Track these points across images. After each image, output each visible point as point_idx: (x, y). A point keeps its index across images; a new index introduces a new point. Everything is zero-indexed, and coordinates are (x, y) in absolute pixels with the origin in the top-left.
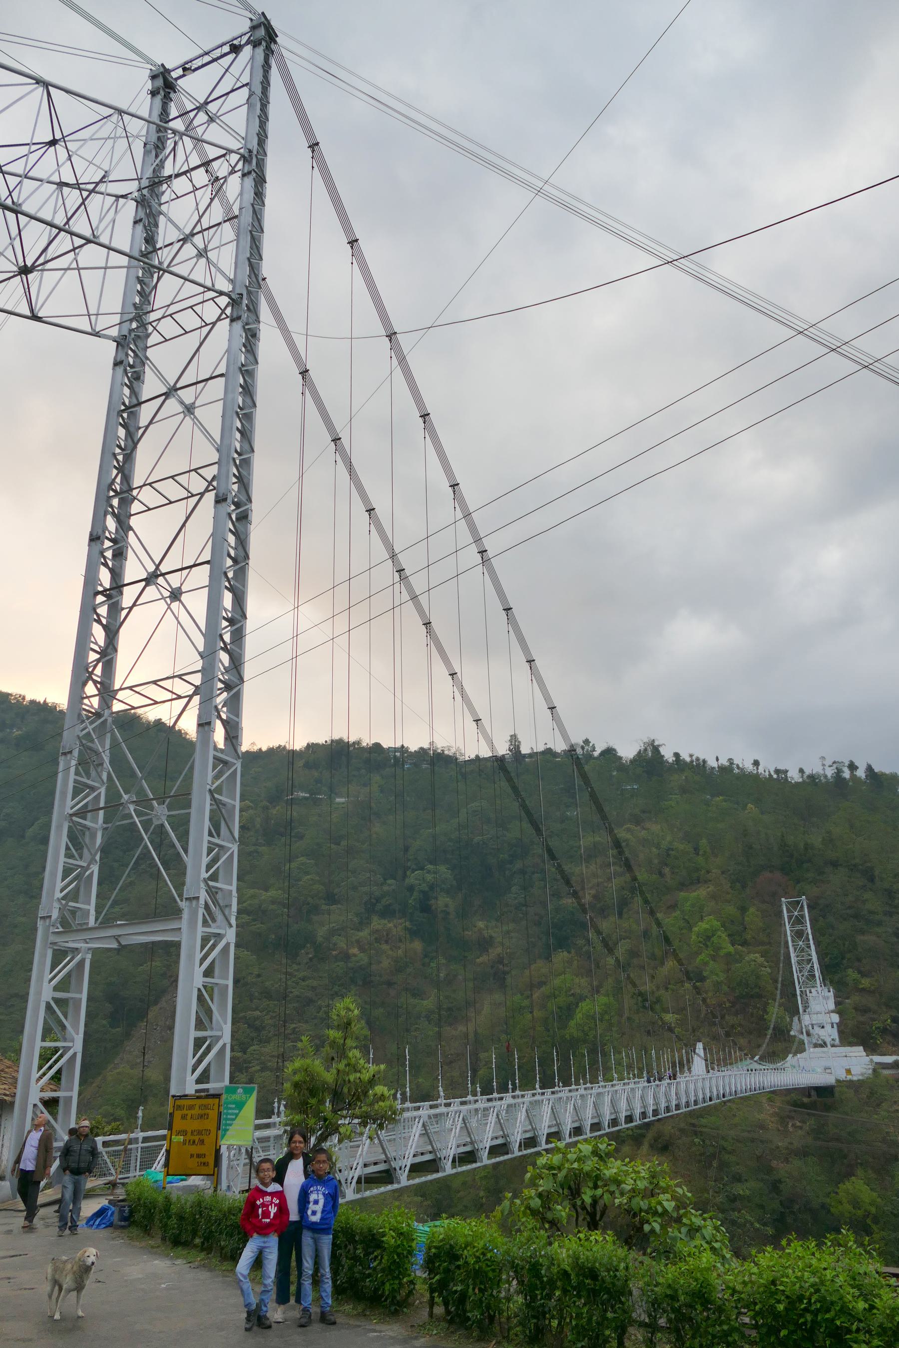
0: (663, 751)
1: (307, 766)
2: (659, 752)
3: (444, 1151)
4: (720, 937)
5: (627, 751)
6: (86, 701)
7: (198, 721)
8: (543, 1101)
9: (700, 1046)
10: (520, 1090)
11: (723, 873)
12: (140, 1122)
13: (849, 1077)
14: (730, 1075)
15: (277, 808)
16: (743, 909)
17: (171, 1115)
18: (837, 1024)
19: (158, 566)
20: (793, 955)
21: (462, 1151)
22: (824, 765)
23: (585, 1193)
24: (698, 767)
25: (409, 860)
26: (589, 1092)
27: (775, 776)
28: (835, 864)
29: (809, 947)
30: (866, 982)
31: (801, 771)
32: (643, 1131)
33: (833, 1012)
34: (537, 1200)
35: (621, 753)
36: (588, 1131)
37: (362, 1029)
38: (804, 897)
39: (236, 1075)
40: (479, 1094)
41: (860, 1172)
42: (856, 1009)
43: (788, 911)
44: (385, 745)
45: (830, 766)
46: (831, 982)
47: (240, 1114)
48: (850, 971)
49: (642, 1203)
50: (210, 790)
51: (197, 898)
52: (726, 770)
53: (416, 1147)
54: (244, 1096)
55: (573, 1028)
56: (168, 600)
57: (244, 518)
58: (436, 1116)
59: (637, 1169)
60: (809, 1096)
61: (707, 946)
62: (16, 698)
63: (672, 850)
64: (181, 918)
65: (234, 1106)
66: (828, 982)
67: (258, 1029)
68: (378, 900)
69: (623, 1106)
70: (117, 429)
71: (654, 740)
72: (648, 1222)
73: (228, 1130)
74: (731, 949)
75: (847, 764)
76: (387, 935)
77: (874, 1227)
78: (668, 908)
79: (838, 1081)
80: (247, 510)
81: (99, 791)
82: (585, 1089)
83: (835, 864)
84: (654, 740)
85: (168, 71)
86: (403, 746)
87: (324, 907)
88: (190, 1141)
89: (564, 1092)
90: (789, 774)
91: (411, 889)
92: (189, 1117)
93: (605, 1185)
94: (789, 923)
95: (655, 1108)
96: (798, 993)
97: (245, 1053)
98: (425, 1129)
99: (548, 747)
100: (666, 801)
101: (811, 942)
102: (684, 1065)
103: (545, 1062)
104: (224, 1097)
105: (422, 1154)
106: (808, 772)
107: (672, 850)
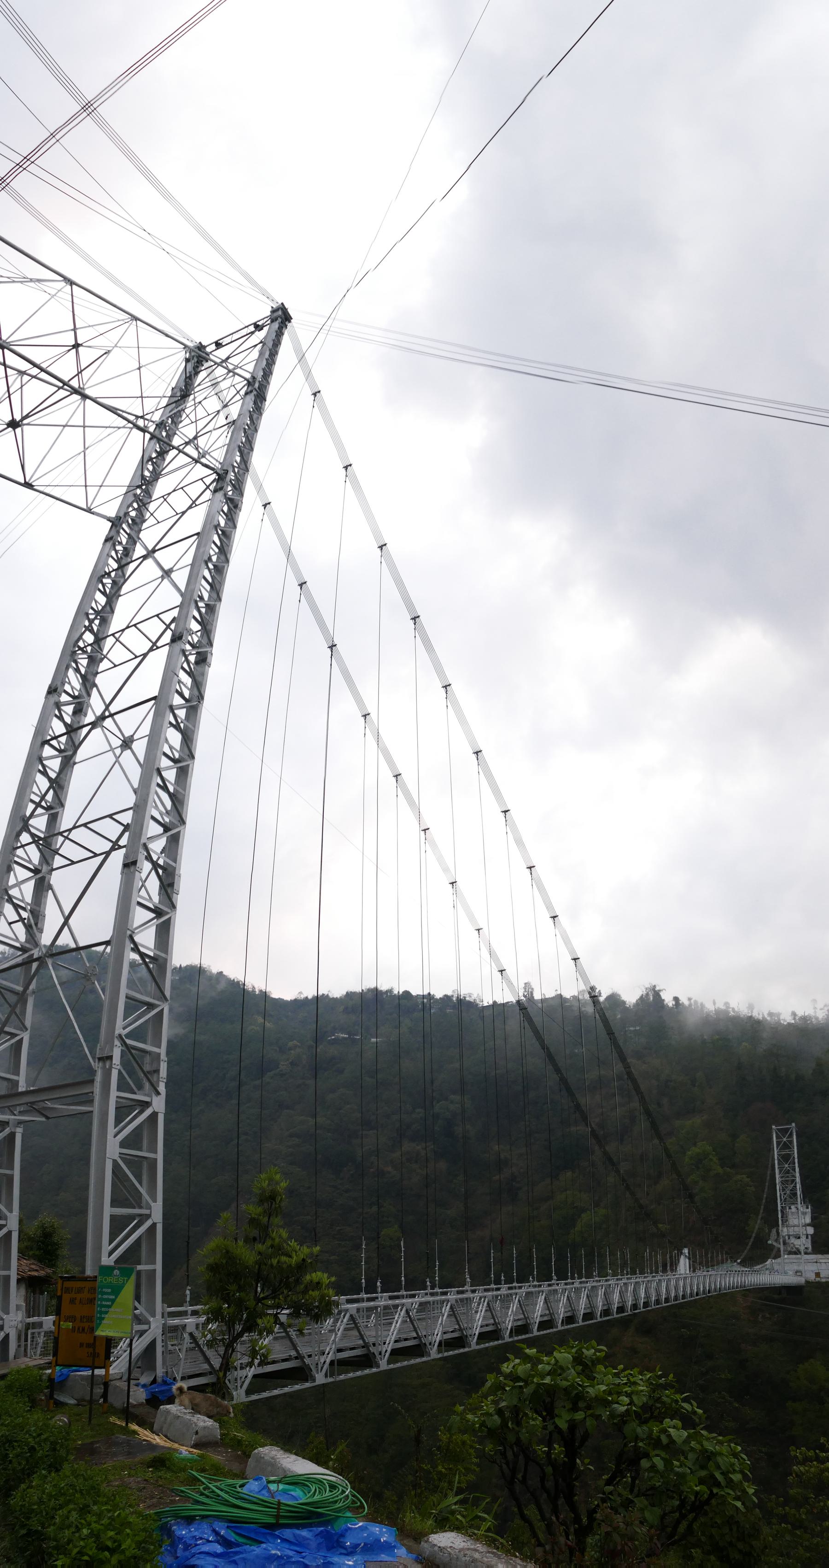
0: (664, 995)
2: (660, 996)
3: (430, 1337)
4: (711, 1160)
5: (630, 997)
6: (20, 852)
7: (124, 861)
8: (474, 1298)
9: (686, 1251)
12: (188, 1299)
13: (818, 1279)
14: (705, 1276)
17: (60, 1299)
18: (811, 1235)
19: (107, 707)
20: (777, 1176)
21: (450, 1337)
22: (815, 1008)
23: (560, 1416)
26: (583, 1285)
29: (794, 1170)
33: (809, 1225)
34: (496, 1417)
36: (580, 1321)
40: (503, 1282)
44: (414, 993)
45: (821, 1009)
47: (118, 1300)
49: (639, 1430)
51: (110, 1058)
53: (397, 1334)
54: (121, 1279)
56: (118, 751)
57: (203, 660)
58: (462, 1300)
59: (632, 1380)
65: (109, 1290)
66: (807, 1200)
69: (616, 1297)
71: (655, 986)
72: (647, 1456)
73: (103, 1318)
74: (720, 1170)
79: (807, 1282)
81: (32, 952)
82: (581, 1283)
84: (655, 986)
85: (205, 347)
86: (429, 994)
88: (79, 1329)
89: (560, 1286)
93: (589, 1407)
94: (777, 1148)
95: (646, 1300)
96: (779, 1208)
98: (453, 1311)
101: (797, 1165)
104: (99, 1279)
105: (406, 1340)
106: (800, 1013)
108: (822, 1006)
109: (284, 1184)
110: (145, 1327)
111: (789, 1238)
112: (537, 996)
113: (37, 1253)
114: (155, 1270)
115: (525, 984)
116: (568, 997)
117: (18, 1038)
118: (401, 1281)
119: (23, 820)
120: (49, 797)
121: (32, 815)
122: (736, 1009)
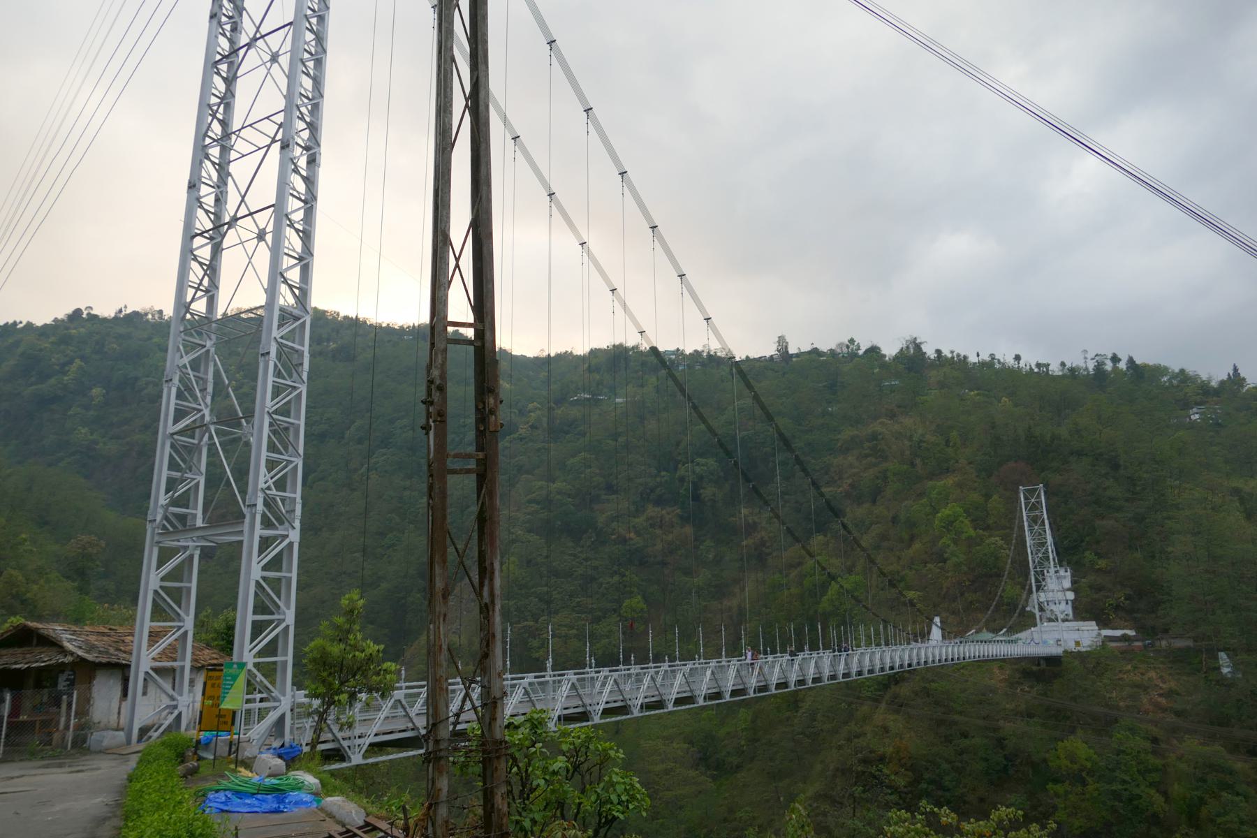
0: (924, 348)
1: (590, 370)
2: (920, 349)
5: (890, 350)
9: (937, 620)
10: (704, 659)
11: (970, 463)
15: (562, 409)
16: (988, 496)
18: (1072, 601)
22: (1086, 358)
24: (960, 363)
25: (680, 454)
27: (1036, 370)
28: (1080, 454)
30: (1102, 563)
31: (1063, 364)
32: (882, 693)
33: (1068, 590)
35: (884, 351)
37: (639, 602)
38: (1041, 485)
39: (529, 641)
41: (1080, 732)
42: (1091, 587)
43: (1026, 498)
46: (1069, 563)
47: (236, 684)
48: (1087, 553)
50: (268, 412)
52: (988, 366)
55: (825, 604)
60: (1039, 664)
61: (949, 531)
62: (331, 315)
63: (924, 442)
64: (243, 522)
65: (230, 678)
66: (1065, 563)
67: (548, 602)
68: (652, 490)
70: (213, 76)
71: (916, 338)
73: (225, 697)
74: (972, 532)
75: (1110, 356)
76: (661, 521)
77: (1089, 780)
78: (918, 496)
80: (315, 153)
83: (1080, 454)
84: (916, 338)
87: (603, 497)
90: (1051, 368)
91: (682, 479)
92: (216, 685)
97: (537, 621)
99: (815, 346)
100: (922, 396)
102: (924, 635)
103: (799, 632)
106: (1068, 365)
107: (924, 442)
108: (1093, 356)
109: (361, 602)
110: (276, 704)
111: (1048, 605)
112: (792, 350)
113: (222, 643)
114: (286, 661)
115: (779, 337)
116: (825, 351)
117: (196, 481)
118: (619, 658)
119: (185, 307)
120: (206, 282)
121: (193, 300)
122: (1002, 360)
